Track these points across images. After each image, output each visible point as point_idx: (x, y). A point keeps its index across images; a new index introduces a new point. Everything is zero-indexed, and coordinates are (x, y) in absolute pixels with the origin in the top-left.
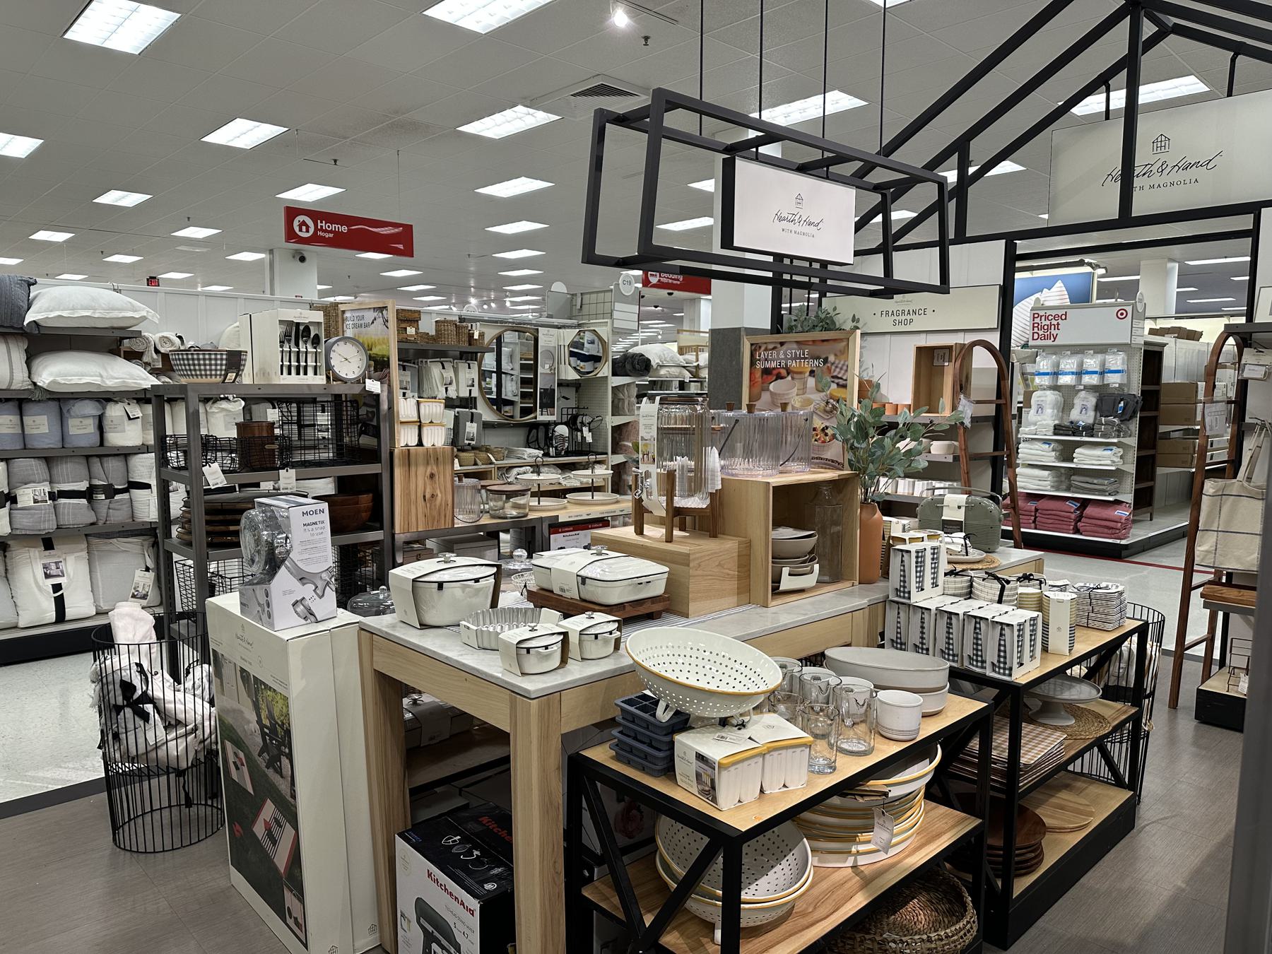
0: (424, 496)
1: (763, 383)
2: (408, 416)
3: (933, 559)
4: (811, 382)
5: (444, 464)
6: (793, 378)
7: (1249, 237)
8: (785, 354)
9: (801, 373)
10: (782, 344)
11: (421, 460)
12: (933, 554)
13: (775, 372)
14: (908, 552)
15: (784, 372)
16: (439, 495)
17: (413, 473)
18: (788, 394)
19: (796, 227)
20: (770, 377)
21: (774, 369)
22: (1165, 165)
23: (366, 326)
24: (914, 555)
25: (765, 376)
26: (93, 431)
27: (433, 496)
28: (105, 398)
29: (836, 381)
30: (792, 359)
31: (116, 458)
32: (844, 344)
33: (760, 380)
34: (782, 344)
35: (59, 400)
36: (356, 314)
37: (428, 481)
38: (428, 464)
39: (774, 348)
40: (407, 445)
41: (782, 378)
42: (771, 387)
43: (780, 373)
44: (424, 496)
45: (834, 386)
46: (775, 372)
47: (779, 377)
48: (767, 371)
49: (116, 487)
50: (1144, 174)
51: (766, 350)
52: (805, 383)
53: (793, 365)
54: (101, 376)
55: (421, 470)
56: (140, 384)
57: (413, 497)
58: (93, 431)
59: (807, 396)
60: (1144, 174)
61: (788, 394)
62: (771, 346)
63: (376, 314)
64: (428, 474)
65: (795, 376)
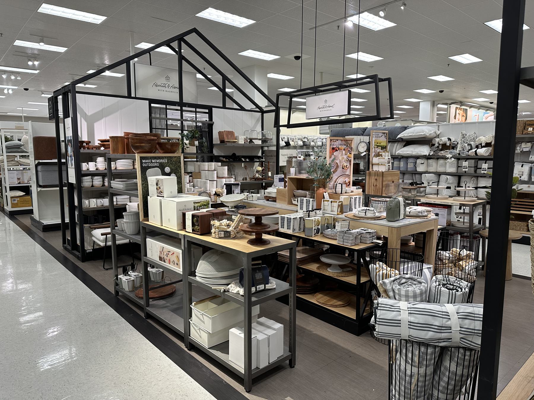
0: (374, 185)
1: (332, 152)
2: (376, 162)
3: (355, 201)
4: (344, 152)
5: (380, 176)
6: (340, 151)
7: (212, 109)
8: (338, 143)
9: (342, 149)
10: (337, 140)
11: (373, 174)
12: (355, 199)
13: (335, 149)
14: (352, 198)
15: (337, 149)
16: (378, 185)
17: (371, 178)
18: (338, 156)
19: (325, 109)
20: (334, 150)
21: (335, 148)
22: (169, 86)
23: (379, 137)
24: (354, 199)
25: (333, 150)
26: (412, 167)
27: (376, 185)
28: (417, 157)
29: (349, 152)
30: (340, 145)
31: (419, 174)
32: (351, 141)
33: (331, 151)
34: (337, 140)
35: (406, 158)
36: (376, 133)
37: (375, 181)
38: (375, 176)
39: (335, 141)
40: (376, 171)
41: (337, 151)
42: (334, 153)
43: (336, 149)
44: (374, 185)
45: (349, 153)
46: (335, 149)
47: (336, 150)
48: (333, 149)
49: (418, 183)
50: (164, 87)
51: (333, 142)
52: (342, 152)
53: (340, 147)
54: (412, 151)
55: (373, 177)
56: (421, 153)
57: (371, 184)
58: (412, 167)
59: (343, 156)
60: (164, 87)
61: (338, 156)
62: (334, 141)
63: (382, 134)
64: (375, 179)
65: (340, 150)
